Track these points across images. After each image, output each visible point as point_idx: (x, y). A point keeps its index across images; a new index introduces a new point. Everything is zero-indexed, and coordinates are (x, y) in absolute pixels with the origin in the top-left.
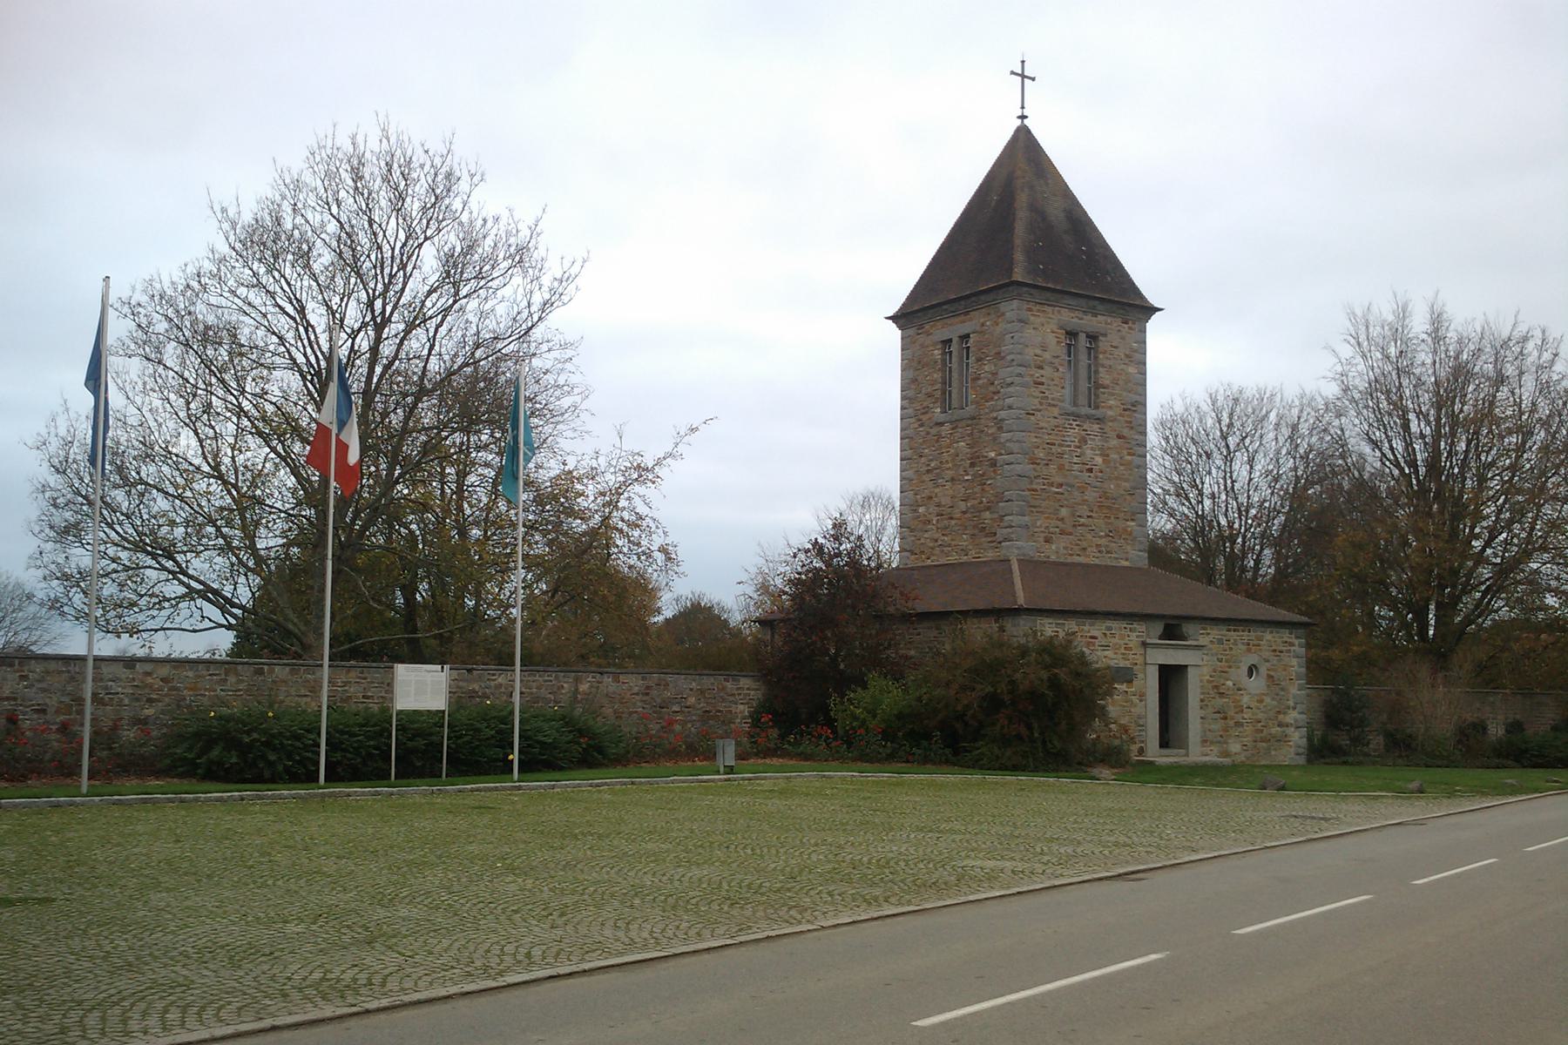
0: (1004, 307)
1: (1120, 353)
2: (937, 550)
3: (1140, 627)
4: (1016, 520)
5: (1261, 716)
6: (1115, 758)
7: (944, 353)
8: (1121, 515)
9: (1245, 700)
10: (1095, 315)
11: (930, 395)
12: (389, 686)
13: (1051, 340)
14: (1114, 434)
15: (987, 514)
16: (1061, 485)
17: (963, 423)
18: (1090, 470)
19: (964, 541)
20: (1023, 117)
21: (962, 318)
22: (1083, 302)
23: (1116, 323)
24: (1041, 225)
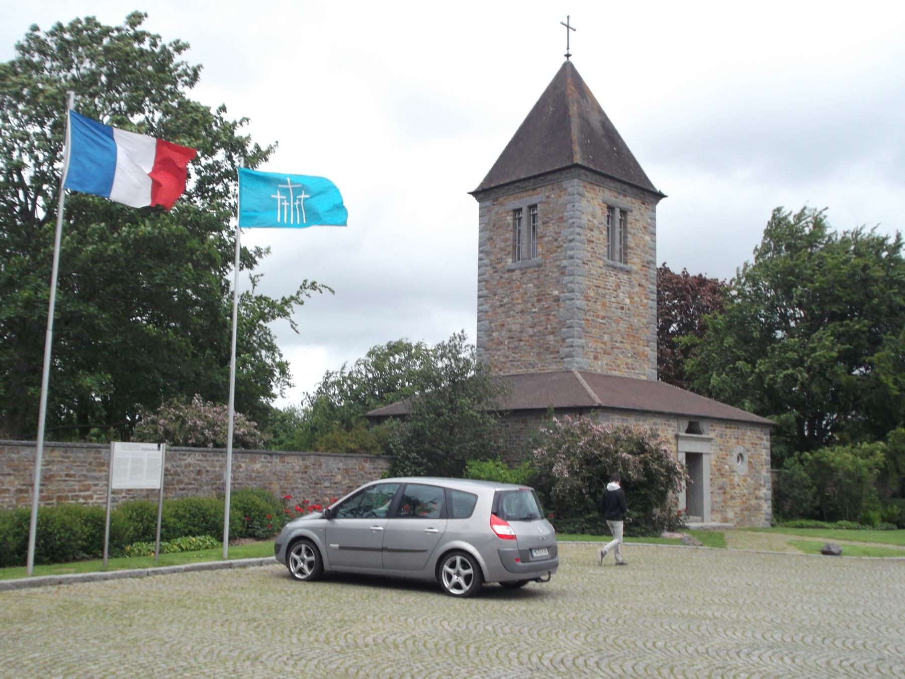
0: (565, 184)
1: (640, 225)
2: (509, 364)
3: (674, 423)
4: (577, 342)
5: (745, 491)
6: (674, 525)
7: (515, 219)
8: (641, 342)
9: (736, 479)
10: (625, 196)
11: (501, 249)
12: (105, 464)
13: (599, 211)
14: (636, 283)
15: (551, 337)
16: (603, 318)
17: (532, 270)
18: (622, 308)
19: (532, 358)
20: (568, 56)
21: (531, 192)
22: (618, 185)
23: (638, 203)
24: (586, 127)
